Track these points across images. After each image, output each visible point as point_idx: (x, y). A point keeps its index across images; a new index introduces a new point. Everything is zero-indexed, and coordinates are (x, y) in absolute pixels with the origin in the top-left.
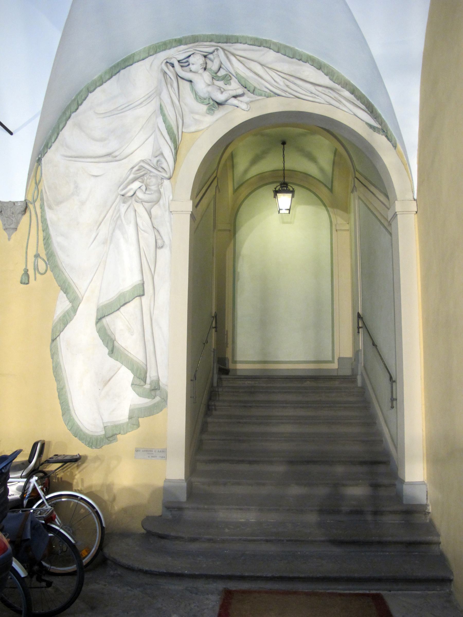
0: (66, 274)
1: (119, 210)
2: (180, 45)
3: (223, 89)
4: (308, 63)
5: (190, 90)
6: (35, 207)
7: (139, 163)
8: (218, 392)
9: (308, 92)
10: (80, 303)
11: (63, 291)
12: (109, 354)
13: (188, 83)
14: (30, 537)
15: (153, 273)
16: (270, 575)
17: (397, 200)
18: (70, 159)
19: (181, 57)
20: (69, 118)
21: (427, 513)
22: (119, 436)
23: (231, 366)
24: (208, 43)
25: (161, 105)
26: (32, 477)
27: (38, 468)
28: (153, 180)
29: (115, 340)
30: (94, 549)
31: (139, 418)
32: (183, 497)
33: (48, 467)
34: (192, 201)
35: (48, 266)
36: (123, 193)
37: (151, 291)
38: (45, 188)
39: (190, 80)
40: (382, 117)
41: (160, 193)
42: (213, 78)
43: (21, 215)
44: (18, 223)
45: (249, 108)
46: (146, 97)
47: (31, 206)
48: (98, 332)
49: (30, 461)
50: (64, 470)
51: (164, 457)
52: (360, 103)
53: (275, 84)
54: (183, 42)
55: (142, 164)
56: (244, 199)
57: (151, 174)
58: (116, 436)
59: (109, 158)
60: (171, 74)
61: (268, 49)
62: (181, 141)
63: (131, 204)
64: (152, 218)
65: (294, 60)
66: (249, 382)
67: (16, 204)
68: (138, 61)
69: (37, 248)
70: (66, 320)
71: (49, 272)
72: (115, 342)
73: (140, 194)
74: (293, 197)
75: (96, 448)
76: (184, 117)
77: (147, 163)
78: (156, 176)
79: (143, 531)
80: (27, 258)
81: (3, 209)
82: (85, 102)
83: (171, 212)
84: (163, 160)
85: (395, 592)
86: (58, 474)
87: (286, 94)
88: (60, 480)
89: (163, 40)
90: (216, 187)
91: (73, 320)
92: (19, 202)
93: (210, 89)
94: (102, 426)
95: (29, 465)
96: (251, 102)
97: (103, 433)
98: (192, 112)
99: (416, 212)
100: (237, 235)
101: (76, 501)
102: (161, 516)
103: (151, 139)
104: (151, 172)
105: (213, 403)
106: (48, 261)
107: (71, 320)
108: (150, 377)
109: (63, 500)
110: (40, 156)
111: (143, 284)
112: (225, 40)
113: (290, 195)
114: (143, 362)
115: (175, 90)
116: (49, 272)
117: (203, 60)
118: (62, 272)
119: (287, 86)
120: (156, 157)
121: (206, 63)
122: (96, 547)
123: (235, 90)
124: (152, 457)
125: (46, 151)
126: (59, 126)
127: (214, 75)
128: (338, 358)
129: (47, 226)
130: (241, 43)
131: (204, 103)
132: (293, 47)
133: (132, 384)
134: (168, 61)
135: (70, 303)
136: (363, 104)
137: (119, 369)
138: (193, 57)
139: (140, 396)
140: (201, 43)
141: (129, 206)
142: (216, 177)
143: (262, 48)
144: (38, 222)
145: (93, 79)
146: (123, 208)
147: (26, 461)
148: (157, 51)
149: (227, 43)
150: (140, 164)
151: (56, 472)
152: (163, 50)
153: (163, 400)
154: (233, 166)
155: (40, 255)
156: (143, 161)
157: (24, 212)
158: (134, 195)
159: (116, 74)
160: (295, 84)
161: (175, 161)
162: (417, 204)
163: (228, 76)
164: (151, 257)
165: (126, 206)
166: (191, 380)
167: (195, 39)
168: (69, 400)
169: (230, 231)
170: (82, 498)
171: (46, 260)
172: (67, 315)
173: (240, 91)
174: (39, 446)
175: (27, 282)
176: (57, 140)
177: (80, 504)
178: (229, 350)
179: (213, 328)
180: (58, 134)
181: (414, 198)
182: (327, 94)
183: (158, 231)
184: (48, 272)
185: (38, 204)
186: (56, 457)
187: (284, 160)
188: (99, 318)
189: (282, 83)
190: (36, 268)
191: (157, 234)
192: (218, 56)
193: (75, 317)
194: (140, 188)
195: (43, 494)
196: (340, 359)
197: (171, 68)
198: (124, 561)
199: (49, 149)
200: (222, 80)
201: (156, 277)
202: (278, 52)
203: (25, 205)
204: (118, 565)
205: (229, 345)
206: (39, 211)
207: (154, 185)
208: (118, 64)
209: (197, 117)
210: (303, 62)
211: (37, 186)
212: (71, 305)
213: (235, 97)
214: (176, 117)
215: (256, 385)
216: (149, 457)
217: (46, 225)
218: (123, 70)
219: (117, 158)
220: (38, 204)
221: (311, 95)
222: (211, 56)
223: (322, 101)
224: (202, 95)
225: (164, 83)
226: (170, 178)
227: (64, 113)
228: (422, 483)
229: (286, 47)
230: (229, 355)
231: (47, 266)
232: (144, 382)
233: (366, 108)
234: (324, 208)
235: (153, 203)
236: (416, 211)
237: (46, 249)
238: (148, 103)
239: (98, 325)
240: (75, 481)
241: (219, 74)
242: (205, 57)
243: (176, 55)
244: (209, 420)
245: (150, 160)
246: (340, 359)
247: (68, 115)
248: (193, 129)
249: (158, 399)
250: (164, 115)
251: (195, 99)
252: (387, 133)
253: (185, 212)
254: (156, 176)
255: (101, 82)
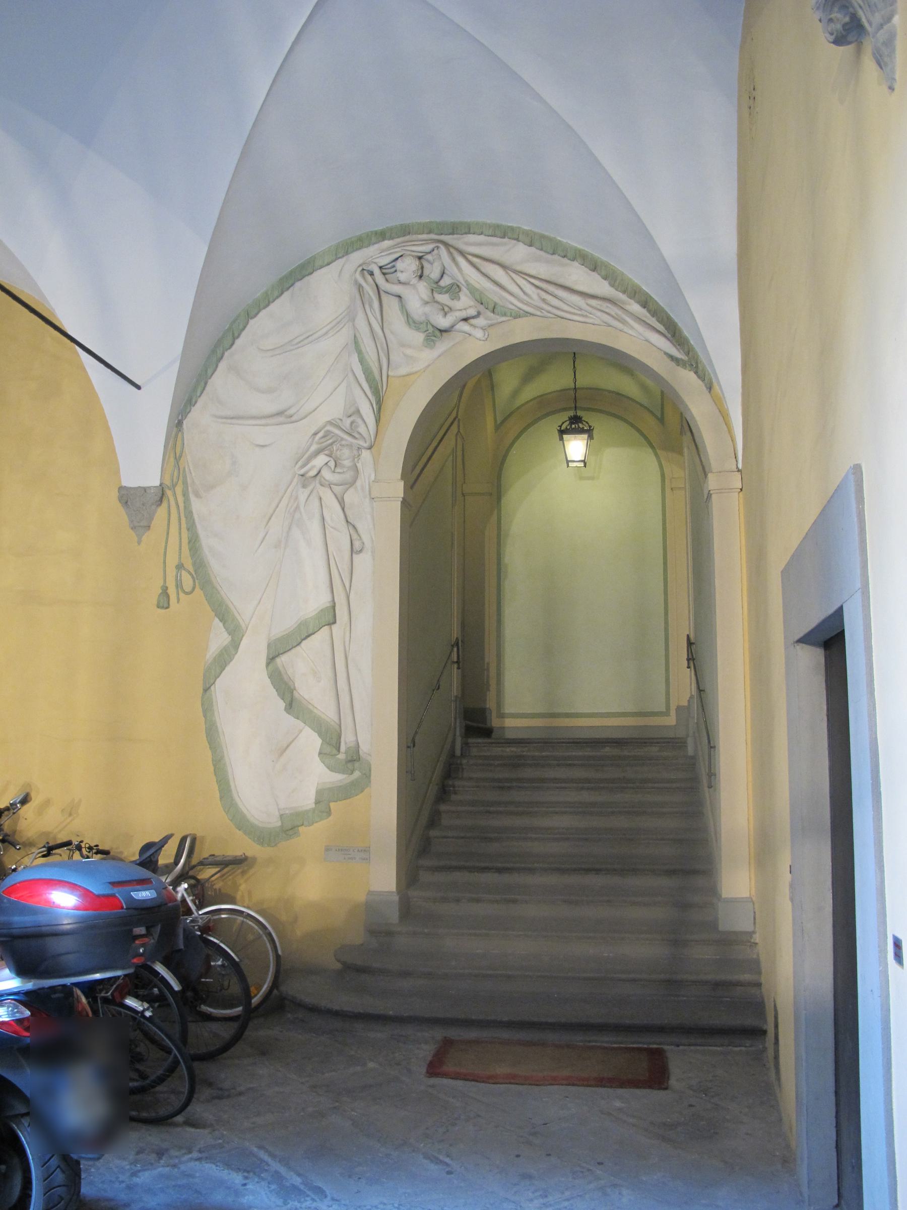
0: (222, 593)
1: (297, 498)
2: (383, 240)
3: (448, 306)
4: (577, 261)
5: (400, 309)
6: (175, 494)
7: (325, 426)
8: (461, 764)
9: (576, 307)
10: (243, 636)
11: (219, 618)
12: (286, 709)
13: (397, 299)
14: (182, 947)
15: (348, 590)
16: (506, 1019)
17: (712, 472)
18: (224, 420)
19: (384, 261)
20: (222, 357)
21: (754, 945)
22: (301, 829)
23: (495, 722)
24: (424, 236)
25: (355, 336)
26: (179, 884)
27: (188, 873)
28: (346, 452)
29: (295, 689)
30: (265, 986)
31: (330, 802)
32: (393, 915)
33: (200, 873)
34: (403, 482)
35: (196, 581)
36: (302, 471)
37: (346, 618)
38: (188, 466)
39: (398, 295)
40: (689, 342)
41: (357, 470)
42: (432, 290)
43: (155, 507)
44: (151, 518)
45: (486, 337)
46: (334, 323)
47: (169, 493)
48: (269, 678)
49: (176, 863)
50: (224, 877)
51: (367, 859)
52: (656, 321)
53: (525, 298)
54: (388, 235)
55: (329, 428)
56: (513, 441)
57: (343, 442)
58: (296, 828)
59: (281, 419)
60: (370, 290)
61: (515, 242)
62: (387, 389)
63: (314, 488)
64: (345, 509)
65: (556, 257)
66: (513, 749)
67: (148, 491)
68: (321, 267)
69: (180, 555)
70: (223, 660)
71: (197, 589)
72: (295, 692)
73: (327, 475)
74: (591, 437)
75: (269, 845)
76: (390, 353)
77: (336, 425)
78: (350, 446)
79: (338, 966)
80: (165, 571)
81: (130, 499)
82: (244, 334)
83: (373, 499)
84: (360, 421)
85: (686, 1048)
86: (214, 884)
87: (541, 312)
88: (218, 892)
89: (358, 234)
90: (457, 435)
91: (234, 661)
92: (152, 488)
93: (427, 309)
94: (277, 813)
95: (175, 868)
96: (489, 326)
97: (279, 824)
98: (403, 345)
99: (741, 490)
100: (503, 501)
101: (241, 918)
102: (362, 945)
103: (344, 384)
104: (342, 439)
105: (450, 783)
106: (195, 574)
107: (231, 660)
108: (346, 743)
109: (223, 916)
110: (180, 418)
111: (334, 607)
112: (451, 231)
113: (586, 436)
114: (335, 720)
115: (375, 313)
116: (197, 589)
117: (416, 265)
118: (217, 590)
119: (544, 300)
120: (350, 416)
121: (422, 268)
122: (269, 983)
123: (465, 309)
124: (349, 858)
125: (188, 410)
126: (206, 371)
127: (435, 286)
128: (676, 707)
129: (194, 522)
130: (474, 234)
131: (420, 331)
132: (554, 236)
133: (320, 753)
134: (365, 268)
135: (230, 635)
136: (661, 324)
137: (301, 731)
138: (400, 261)
139: (331, 770)
140: (414, 237)
141: (311, 492)
142: (455, 419)
143: (506, 240)
144: (180, 517)
145: (256, 297)
146: (303, 494)
147: (171, 864)
148: (349, 250)
149: (453, 234)
150: (326, 429)
151: (213, 881)
152: (357, 249)
153: (365, 776)
154: (492, 388)
155: (185, 566)
156: (330, 423)
157: (159, 503)
158: (319, 475)
159: (288, 289)
160: (555, 296)
161: (378, 421)
162: (742, 478)
163: (455, 287)
164: (344, 566)
165: (307, 491)
166: (408, 747)
167: (405, 231)
168: (230, 776)
169: (491, 494)
170: (249, 915)
171: (193, 573)
172: (225, 653)
173: (472, 312)
174: (189, 842)
175: (166, 605)
176: (205, 392)
177: (246, 922)
178: (491, 696)
179: (454, 662)
180: (206, 384)
181: (737, 468)
182: (604, 310)
183: (354, 527)
184: (196, 590)
185: (179, 490)
186: (213, 857)
187: (575, 377)
188: (271, 657)
189: (535, 297)
190: (179, 585)
191: (352, 531)
192: (440, 257)
193: (236, 657)
194: (326, 464)
195: (195, 908)
196: (679, 708)
197: (369, 278)
198: (308, 1000)
199: (194, 406)
200: (446, 292)
201: (352, 596)
202: (531, 246)
203: (161, 492)
204: (300, 1005)
205: (491, 688)
206: (181, 499)
207: (347, 459)
208: (291, 273)
209: (409, 352)
210: (570, 259)
211: (178, 463)
212: (231, 639)
213: (465, 320)
214: (378, 354)
215: (524, 753)
216: (345, 859)
217: (192, 521)
218: (299, 282)
219: (294, 419)
220: (179, 490)
221: (579, 312)
222: (429, 257)
223: (597, 321)
224: (416, 317)
225: (359, 302)
226: (370, 448)
227: (214, 351)
228: (750, 900)
229: (543, 237)
230: (491, 704)
231: (194, 581)
232: (336, 749)
233: (664, 329)
234: (650, 450)
235: (347, 486)
236: (741, 488)
237: (192, 556)
238: (337, 332)
239: (270, 667)
240: (240, 893)
241: (442, 283)
242: (420, 258)
243: (376, 258)
244: (443, 807)
245: (341, 420)
246: (679, 708)
247: (219, 355)
248: (403, 371)
249: (357, 774)
250: (359, 352)
251: (406, 322)
252: (697, 367)
253: (393, 499)
254: (350, 446)
255: (267, 302)
